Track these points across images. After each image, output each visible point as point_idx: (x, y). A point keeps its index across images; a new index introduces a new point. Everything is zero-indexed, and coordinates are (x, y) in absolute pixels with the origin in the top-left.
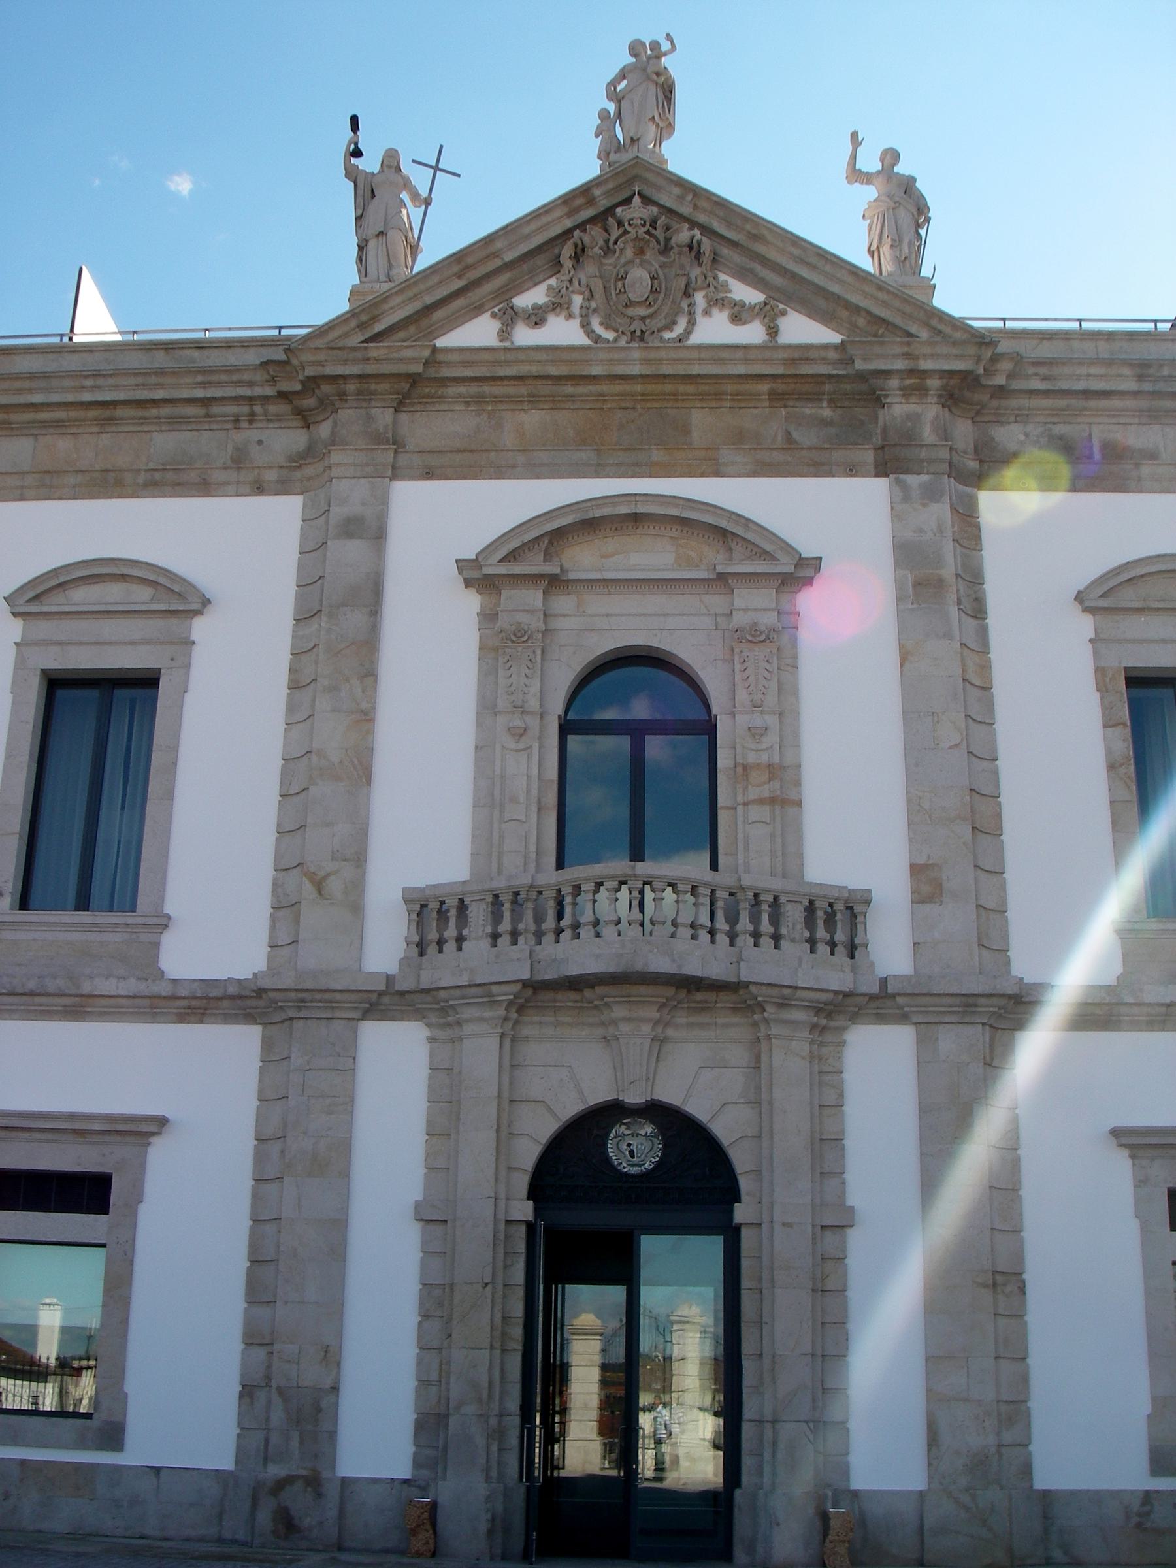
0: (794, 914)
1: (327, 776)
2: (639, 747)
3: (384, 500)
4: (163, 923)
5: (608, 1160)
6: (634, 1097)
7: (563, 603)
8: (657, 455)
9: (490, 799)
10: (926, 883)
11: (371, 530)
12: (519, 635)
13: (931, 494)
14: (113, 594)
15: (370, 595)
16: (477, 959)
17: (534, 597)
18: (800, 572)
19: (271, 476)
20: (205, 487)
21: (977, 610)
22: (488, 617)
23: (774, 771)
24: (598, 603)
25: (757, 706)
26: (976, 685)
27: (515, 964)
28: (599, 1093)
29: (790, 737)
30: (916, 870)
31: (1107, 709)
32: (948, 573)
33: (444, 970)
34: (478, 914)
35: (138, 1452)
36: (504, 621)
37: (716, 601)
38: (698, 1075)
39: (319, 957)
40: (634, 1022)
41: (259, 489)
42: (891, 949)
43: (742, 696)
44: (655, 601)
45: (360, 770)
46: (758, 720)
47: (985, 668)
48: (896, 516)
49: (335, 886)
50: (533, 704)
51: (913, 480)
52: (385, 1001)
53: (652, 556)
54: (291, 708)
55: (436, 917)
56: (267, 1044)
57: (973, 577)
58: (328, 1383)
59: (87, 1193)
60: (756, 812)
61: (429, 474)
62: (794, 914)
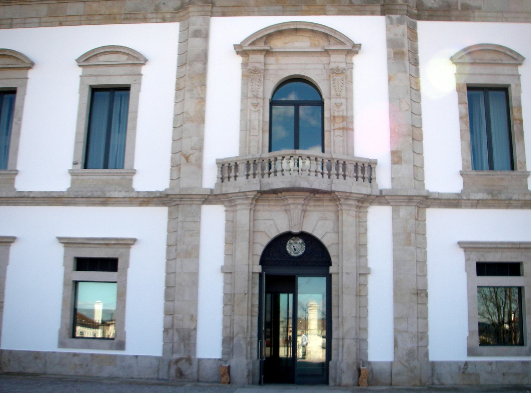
0: (350, 168)
1: (189, 121)
2: (298, 109)
3: (208, 24)
4: (133, 172)
5: (286, 252)
6: (296, 230)
7: (271, 60)
8: (304, 8)
9: (246, 128)
10: (396, 157)
11: (203, 34)
12: (255, 71)
13: (400, 22)
14: (113, 58)
15: (203, 57)
16: (243, 183)
17: (261, 58)
18: (354, 49)
19: (168, 16)
20: (145, 20)
21: (416, 63)
22: (245, 65)
23: (344, 118)
24: (283, 60)
25: (338, 96)
26: (415, 90)
27: (254, 184)
28: (284, 229)
29: (350, 106)
30: (393, 153)
31: (460, 98)
32: (406, 49)
33: (230, 187)
34: (242, 168)
35: (130, 350)
36: (250, 66)
37: (324, 59)
38: (318, 223)
39: (186, 183)
40: (295, 205)
41: (164, 20)
42: (384, 180)
43: (333, 92)
44: (303, 59)
45: (200, 119)
46: (338, 101)
47: (418, 83)
48: (388, 29)
49: (192, 159)
50: (261, 95)
51: (394, 17)
52: (210, 198)
53: (302, 43)
54: (177, 97)
55: (227, 169)
56: (170, 213)
57: (414, 51)
58: (193, 327)
59: (109, 265)
60: (337, 133)
61: (224, 14)
62: (350, 168)
